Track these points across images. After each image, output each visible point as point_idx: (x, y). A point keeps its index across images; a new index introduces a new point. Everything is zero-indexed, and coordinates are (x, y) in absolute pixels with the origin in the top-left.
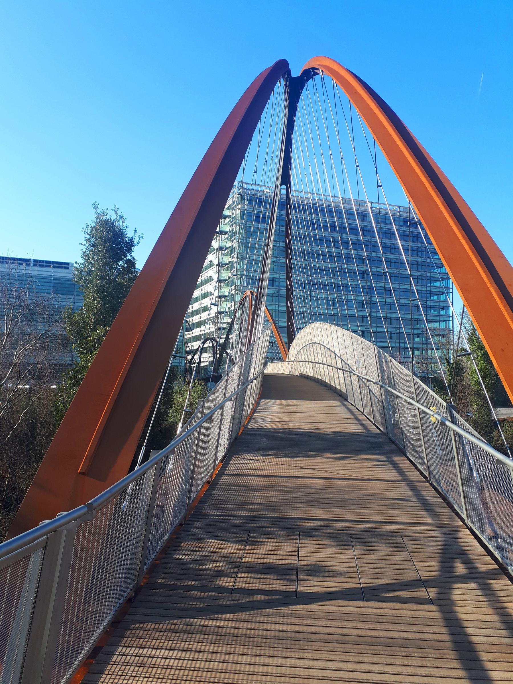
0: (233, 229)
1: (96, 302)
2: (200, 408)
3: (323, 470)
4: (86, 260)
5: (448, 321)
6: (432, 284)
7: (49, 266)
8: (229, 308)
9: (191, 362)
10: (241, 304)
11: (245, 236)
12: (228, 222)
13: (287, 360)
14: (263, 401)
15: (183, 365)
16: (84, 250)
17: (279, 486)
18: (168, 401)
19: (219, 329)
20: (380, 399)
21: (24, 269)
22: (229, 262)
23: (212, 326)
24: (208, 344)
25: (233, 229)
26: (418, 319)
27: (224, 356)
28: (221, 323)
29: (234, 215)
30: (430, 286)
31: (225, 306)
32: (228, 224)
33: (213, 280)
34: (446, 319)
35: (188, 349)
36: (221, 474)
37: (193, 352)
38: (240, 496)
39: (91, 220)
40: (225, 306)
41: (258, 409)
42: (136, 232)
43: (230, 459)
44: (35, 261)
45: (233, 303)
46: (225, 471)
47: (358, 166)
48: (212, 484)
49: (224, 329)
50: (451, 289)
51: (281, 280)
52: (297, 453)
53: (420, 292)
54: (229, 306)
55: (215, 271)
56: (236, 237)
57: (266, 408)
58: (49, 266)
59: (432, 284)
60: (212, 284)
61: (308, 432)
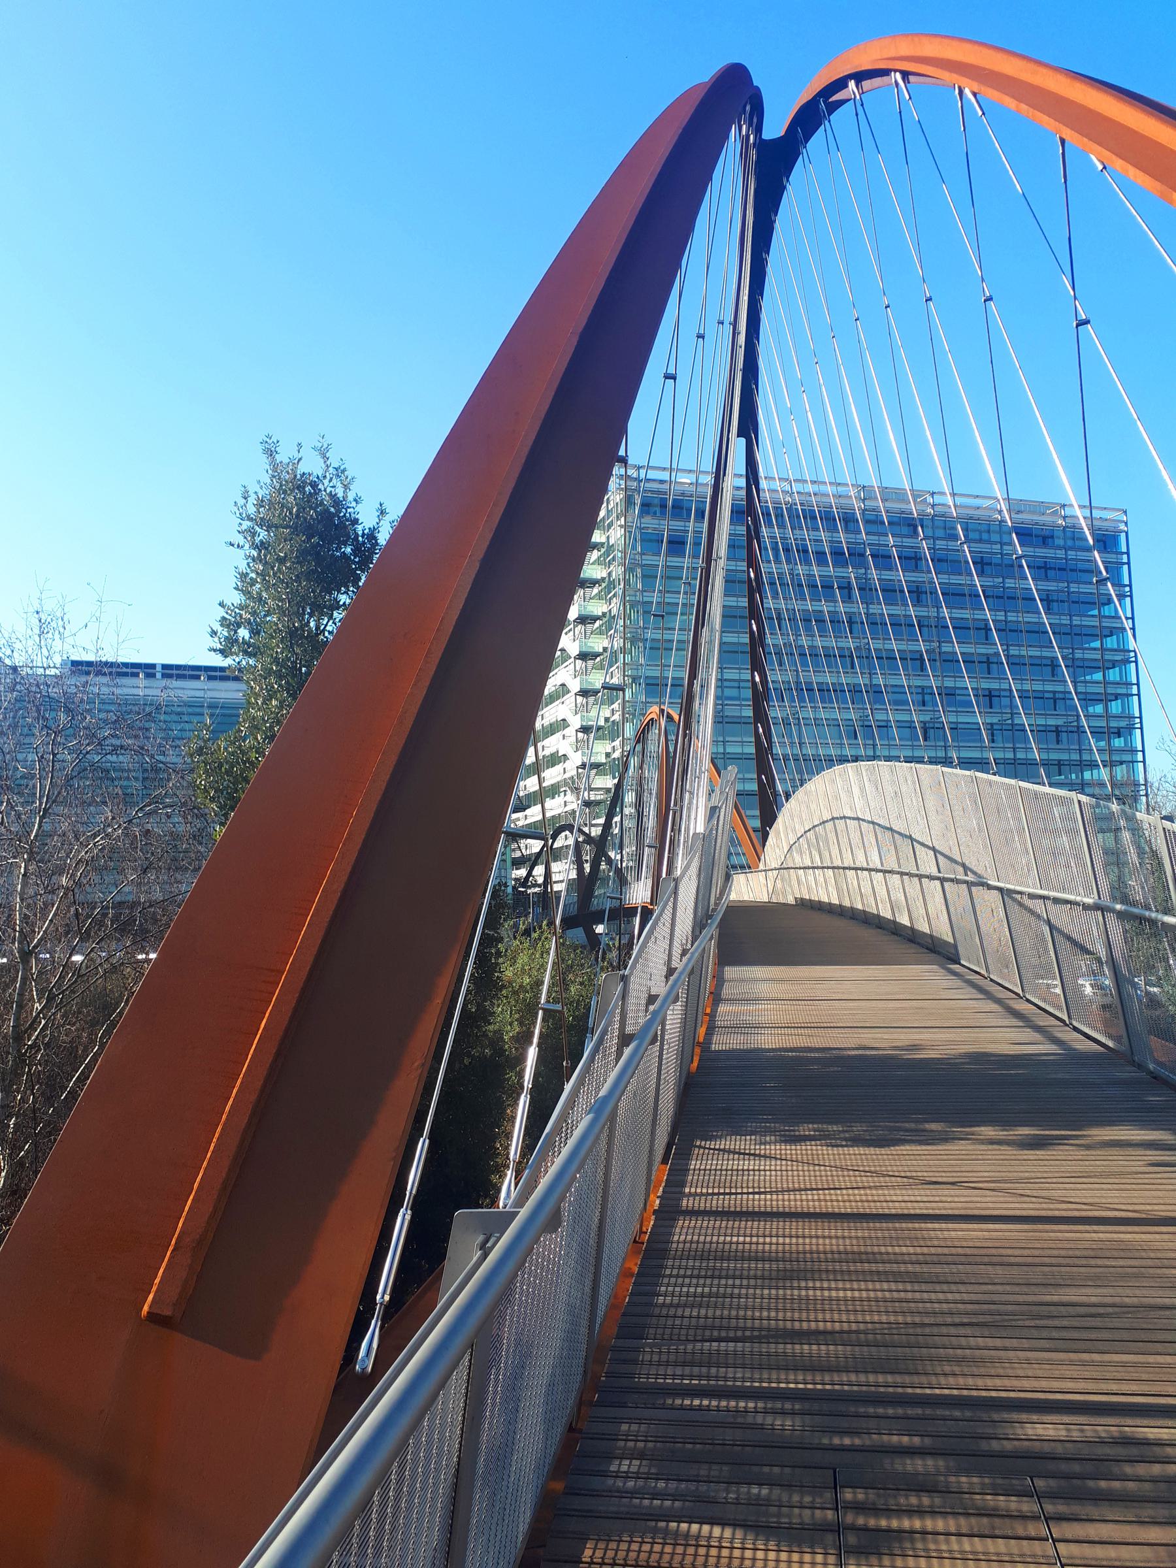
0: (610, 574)
1: (274, 702)
2: (615, 1007)
3: (995, 1186)
4: (246, 593)
5: (1133, 762)
6: (1088, 678)
7: (198, 677)
8: (608, 755)
9: (524, 882)
10: (638, 742)
11: (639, 586)
12: (599, 558)
13: (761, 867)
14: (730, 972)
15: (509, 890)
16: (243, 567)
17: (871, 1258)
18: (487, 981)
19: (587, 804)
20: (1103, 954)
21: (139, 687)
22: (605, 649)
23: (570, 797)
24: (565, 840)
25: (610, 574)
26: (1059, 761)
27: (603, 866)
28: (591, 789)
29: (612, 541)
30: (1086, 682)
31: (601, 750)
32: (598, 562)
33: (569, 692)
34: (1127, 757)
35: (518, 854)
36: (670, 1212)
37: (529, 860)
38: (764, 1305)
39: (257, 478)
40: (601, 750)
41: (726, 992)
42: (383, 512)
43: (685, 1154)
44: (164, 667)
45: (617, 743)
46: (680, 1199)
47: (990, 299)
48: (653, 1252)
49: (598, 803)
50: (1135, 687)
51: (726, 684)
52: (891, 1129)
53: (1061, 696)
54: (609, 750)
55: (572, 672)
56: (619, 589)
57: (745, 988)
58: (198, 677)
59: (1088, 678)
60: (567, 702)
61: (891, 1057)
